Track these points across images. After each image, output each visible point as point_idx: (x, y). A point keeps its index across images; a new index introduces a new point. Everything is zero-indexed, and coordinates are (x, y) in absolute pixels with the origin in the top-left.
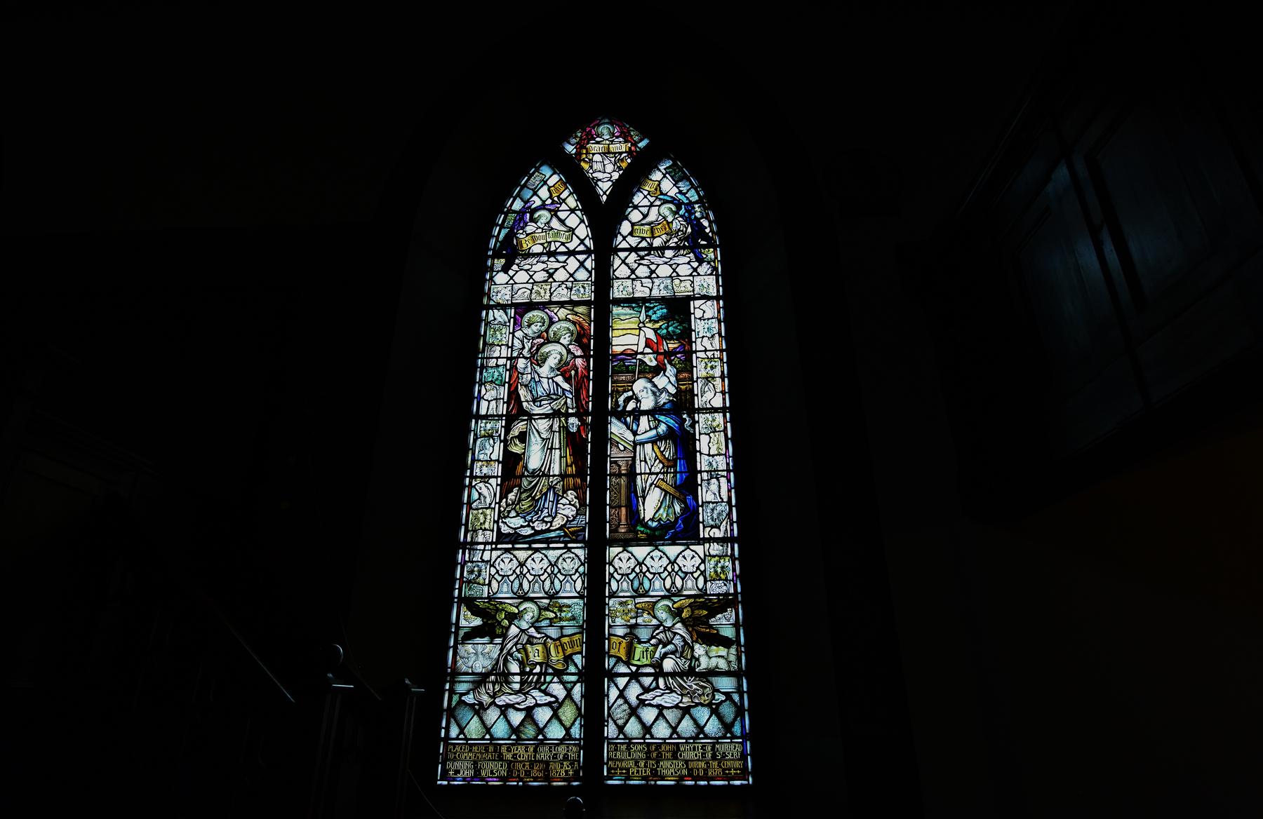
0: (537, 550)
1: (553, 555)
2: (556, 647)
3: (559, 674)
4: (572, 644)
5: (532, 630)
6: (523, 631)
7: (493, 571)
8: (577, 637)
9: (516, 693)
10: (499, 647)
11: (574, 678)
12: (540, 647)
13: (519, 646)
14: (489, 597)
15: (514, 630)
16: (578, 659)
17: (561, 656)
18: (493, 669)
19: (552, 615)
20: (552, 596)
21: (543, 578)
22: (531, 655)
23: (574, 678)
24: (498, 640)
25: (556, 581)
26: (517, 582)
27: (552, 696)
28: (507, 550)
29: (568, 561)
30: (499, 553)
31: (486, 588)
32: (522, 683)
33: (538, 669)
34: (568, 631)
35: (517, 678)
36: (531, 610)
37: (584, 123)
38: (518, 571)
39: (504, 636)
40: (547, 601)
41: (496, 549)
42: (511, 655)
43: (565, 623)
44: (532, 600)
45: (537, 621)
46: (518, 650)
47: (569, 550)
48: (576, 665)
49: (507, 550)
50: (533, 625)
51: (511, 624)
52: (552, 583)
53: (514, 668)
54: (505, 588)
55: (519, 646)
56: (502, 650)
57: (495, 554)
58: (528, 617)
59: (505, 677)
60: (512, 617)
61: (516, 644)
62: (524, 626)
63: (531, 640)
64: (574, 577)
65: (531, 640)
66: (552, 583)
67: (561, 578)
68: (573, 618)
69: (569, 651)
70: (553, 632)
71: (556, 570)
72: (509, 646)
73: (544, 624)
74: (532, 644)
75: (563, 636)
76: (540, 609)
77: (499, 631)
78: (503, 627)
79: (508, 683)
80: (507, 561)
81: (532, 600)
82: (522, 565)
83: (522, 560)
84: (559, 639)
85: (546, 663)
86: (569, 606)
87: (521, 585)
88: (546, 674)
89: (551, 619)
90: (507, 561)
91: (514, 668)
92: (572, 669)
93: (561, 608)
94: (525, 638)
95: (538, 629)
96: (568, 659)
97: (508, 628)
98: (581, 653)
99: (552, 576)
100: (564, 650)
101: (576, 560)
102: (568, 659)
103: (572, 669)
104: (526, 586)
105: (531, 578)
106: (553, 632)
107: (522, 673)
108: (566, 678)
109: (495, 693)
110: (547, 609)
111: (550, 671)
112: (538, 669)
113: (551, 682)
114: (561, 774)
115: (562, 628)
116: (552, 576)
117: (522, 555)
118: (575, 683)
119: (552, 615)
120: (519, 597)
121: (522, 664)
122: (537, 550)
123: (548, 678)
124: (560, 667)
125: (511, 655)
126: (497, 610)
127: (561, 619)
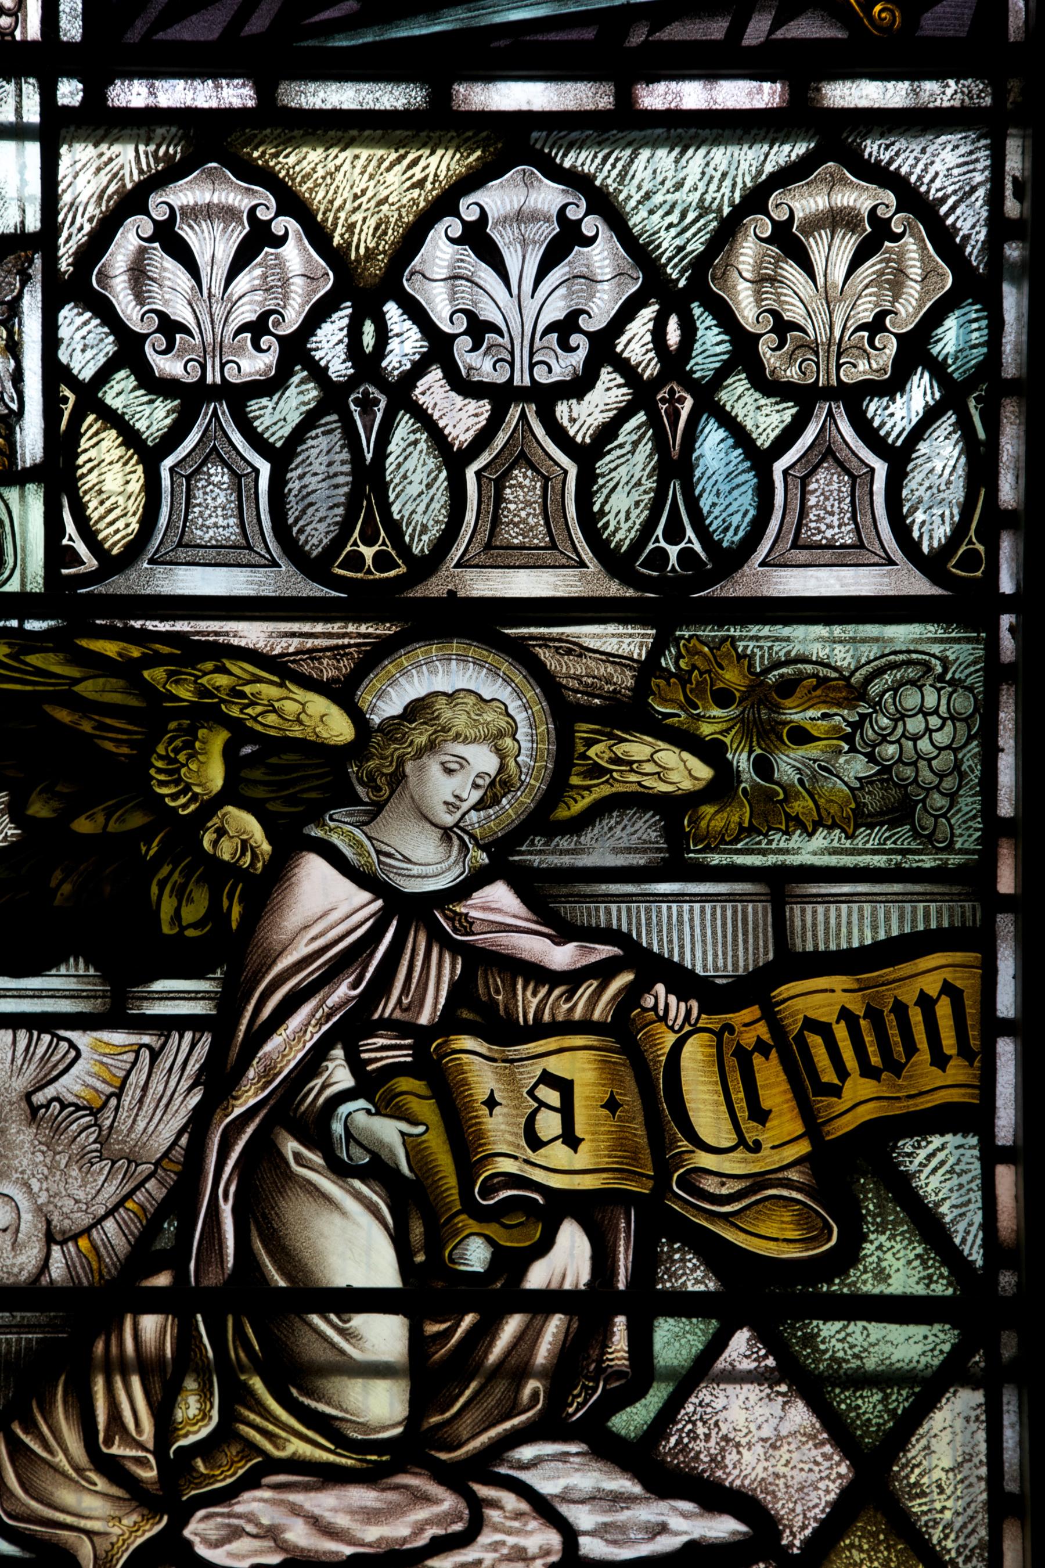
0: (513, 144)
1: (672, 188)
2: (735, 1065)
3: (772, 1303)
4: (886, 1039)
5: (499, 899)
6: (407, 911)
7: (85, 346)
8: (930, 973)
9: (377, 1462)
10: (190, 1052)
11: (908, 1345)
12: (579, 1065)
13: (382, 1050)
14: (61, 591)
15: (322, 902)
16: (941, 1169)
17: (783, 1141)
18: (143, 1255)
19: (682, 771)
20: (679, 589)
21: (582, 417)
22: (500, 1130)
23: (908, 1345)
24: (181, 996)
25: (713, 447)
26: (323, 452)
27: (714, 1496)
28: (205, 141)
29: (833, 254)
30: (128, 160)
31: (29, 510)
32: (428, 1376)
33: (567, 1260)
34: (849, 922)
35: (384, 1336)
36: (470, 729)
37: (549, 1024)
38: (330, 343)
39: (233, 946)
40: (629, 641)
41: (100, 121)
42: (315, 1131)
43: (810, 850)
44: (486, 626)
45: (541, 822)
46: (369, 1085)
47: (839, 141)
48: (929, 1228)
49: (205, 141)
50: (501, 861)
51: (290, 844)
52: (675, 467)
53: (353, 1245)
54: (214, 511)
55: (382, 1050)
56: (218, 1080)
57: (90, 172)
58: (452, 781)
59: (270, 1322)
60: (313, 791)
61: (350, 1030)
62: (426, 863)
63: (487, 999)
64: (899, 414)
65: (487, 999)
66: (675, 467)
67: (766, 419)
68: (891, 803)
69: (859, 1101)
70: (699, 931)
71: (711, 343)
72: (286, 1046)
73: (603, 848)
74: (504, 1031)
75: (792, 963)
76: (564, 709)
77: (178, 910)
78: (217, 874)
79: (297, 1376)
80: (213, 245)
81: (486, 626)
82: (367, 285)
83: (364, 235)
84: (754, 988)
85: (648, 1205)
86: (845, 689)
87: (369, 480)
88: (648, 1304)
89: (672, 809)
90: (213, 245)
91: (353, 1245)
92: (896, 1264)
93: (765, 701)
94: (430, 986)
95: (549, 900)
96: (852, 1174)
97: (266, 886)
98: (972, 1117)
99: (670, 399)
100: (808, 1090)
101: (913, 251)
102: (852, 1174)
103: (896, 1264)
104: (415, 487)
105: (462, 418)
106: (699, 931)
107: (424, 1290)
108: (837, 1339)
109: (177, 1467)
110: (628, 713)
111: (693, 1277)
112: (567, 1260)
113: (701, 1370)
114: (633, 363)
115: (782, 885)
116: (670, 399)
117: (364, 187)
118: (927, 1389)
119: (682, 771)
120: (359, 601)
121: (409, 1203)
122: (513, 144)
123: (674, 1341)
124: (774, 1237)
125: (315, 1131)
126: (154, 715)
127: (773, 811)
